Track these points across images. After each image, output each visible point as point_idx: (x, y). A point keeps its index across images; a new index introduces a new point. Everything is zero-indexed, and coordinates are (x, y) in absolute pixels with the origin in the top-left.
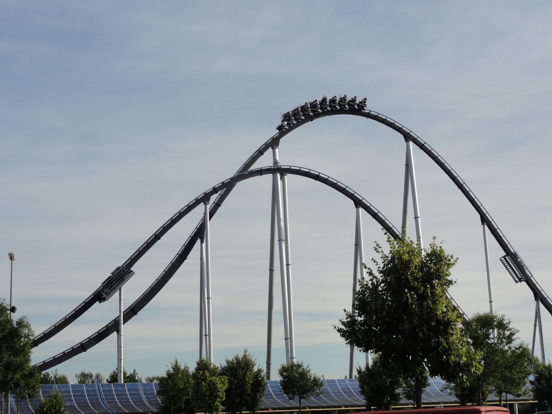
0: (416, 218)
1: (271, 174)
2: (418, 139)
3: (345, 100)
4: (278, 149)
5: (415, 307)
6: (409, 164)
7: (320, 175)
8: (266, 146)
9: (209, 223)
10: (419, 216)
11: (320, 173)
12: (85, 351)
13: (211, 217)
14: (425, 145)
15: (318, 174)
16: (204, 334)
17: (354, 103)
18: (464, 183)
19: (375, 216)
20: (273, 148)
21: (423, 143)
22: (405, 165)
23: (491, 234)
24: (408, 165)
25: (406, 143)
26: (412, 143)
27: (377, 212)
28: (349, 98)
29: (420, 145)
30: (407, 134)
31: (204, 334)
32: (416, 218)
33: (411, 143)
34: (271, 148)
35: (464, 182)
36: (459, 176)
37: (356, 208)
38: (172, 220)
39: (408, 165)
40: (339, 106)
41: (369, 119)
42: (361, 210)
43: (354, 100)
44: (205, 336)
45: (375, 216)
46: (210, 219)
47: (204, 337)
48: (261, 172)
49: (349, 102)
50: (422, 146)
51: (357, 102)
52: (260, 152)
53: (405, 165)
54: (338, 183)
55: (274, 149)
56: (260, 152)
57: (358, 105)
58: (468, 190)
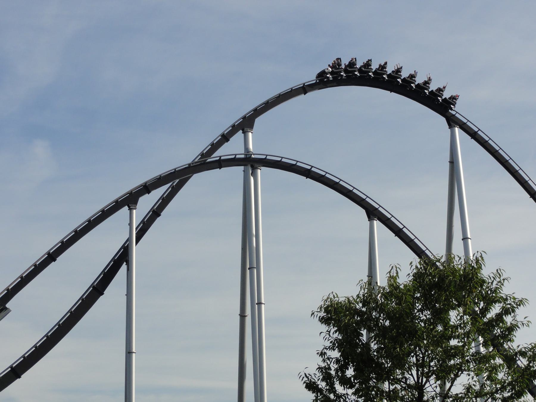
0: (465, 239)
1: (6, 306)
2: (468, 124)
3: (340, 65)
4: (252, 133)
5: (462, 360)
6: (454, 161)
7: (313, 169)
8: (234, 129)
9: (135, 249)
10: (469, 236)
11: (312, 167)
12: (20, 377)
13: (138, 240)
14: (479, 132)
15: (309, 167)
16: (248, 266)
17: (368, 68)
18: (479, 130)
19: (399, 232)
20: (244, 132)
21: (476, 130)
22: (449, 162)
23: (531, 198)
24: (453, 163)
25: (449, 130)
26: (458, 129)
27: (401, 226)
28: (345, 62)
29: (472, 132)
30: (452, 116)
31: (248, 266)
32: (465, 239)
33: (457, 130)
34: (241, 131)
35: (478, 128)
36: (470, 120)
37: (369, 221)
38: (163, 199)
39: (453, 163)
40: (345, 73)
41: (105, 292)
42: (376, 223)
43: (352, 64)
44: (249, 269)
45: (399, 232)
46: (137, 242)
47: (248, 271)
48: (233, 162)
49: (346, 66)
50: (474, 135)
51: (358, 66)
52: (225, 138)
53: (449, 162)
54: (341, 183)
55: (246, 133)
56: (225, 138)
57: (360, 70)
58: (507, 158)
